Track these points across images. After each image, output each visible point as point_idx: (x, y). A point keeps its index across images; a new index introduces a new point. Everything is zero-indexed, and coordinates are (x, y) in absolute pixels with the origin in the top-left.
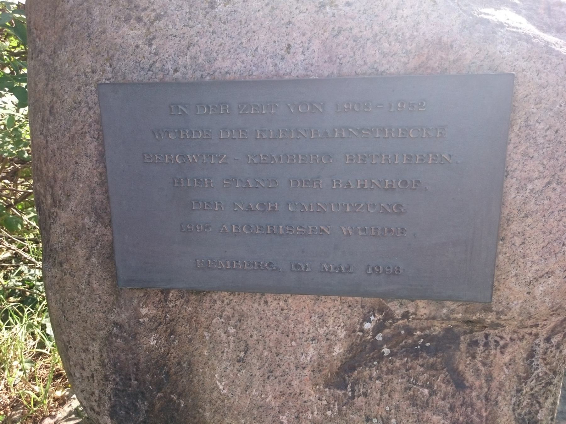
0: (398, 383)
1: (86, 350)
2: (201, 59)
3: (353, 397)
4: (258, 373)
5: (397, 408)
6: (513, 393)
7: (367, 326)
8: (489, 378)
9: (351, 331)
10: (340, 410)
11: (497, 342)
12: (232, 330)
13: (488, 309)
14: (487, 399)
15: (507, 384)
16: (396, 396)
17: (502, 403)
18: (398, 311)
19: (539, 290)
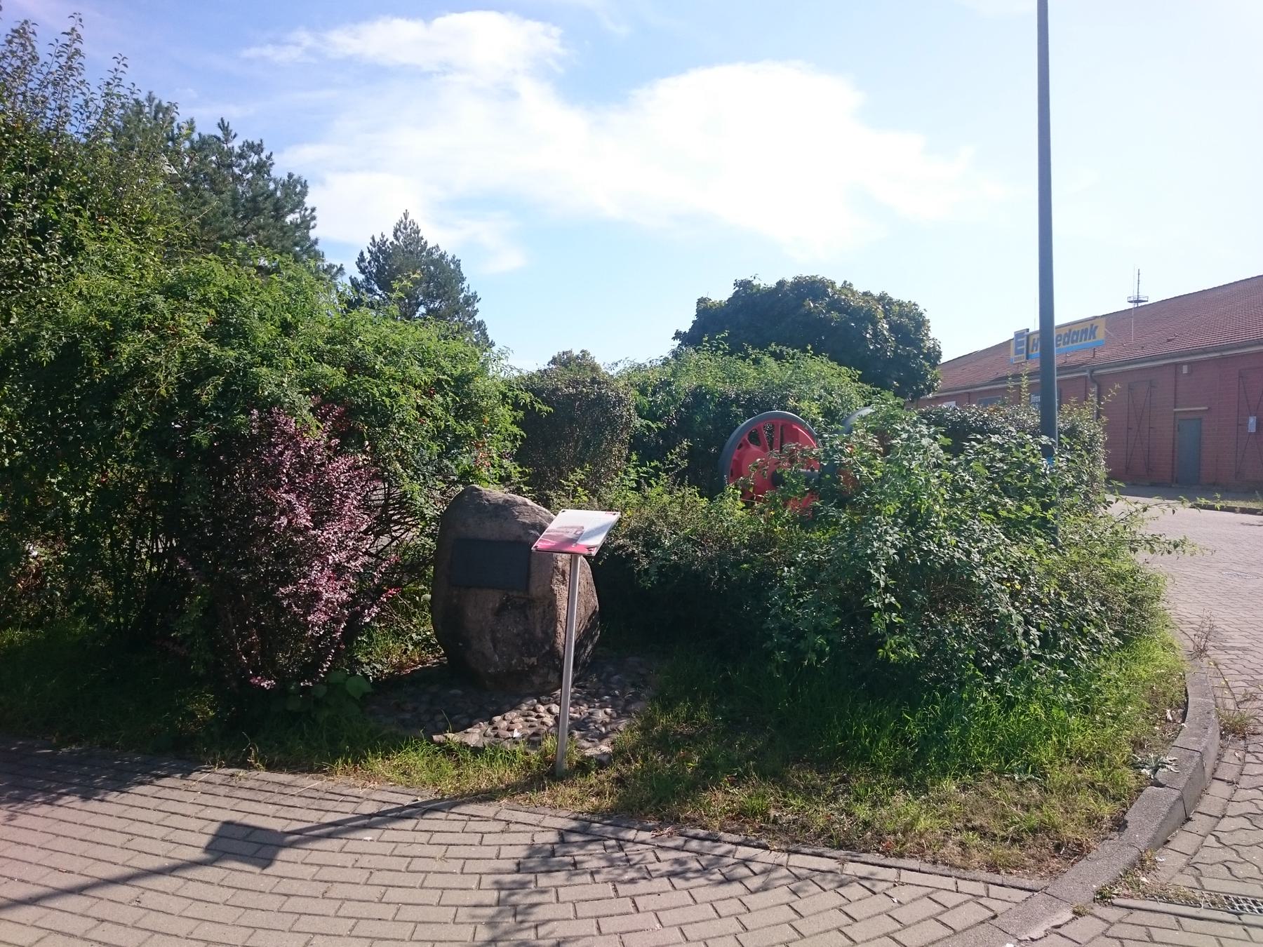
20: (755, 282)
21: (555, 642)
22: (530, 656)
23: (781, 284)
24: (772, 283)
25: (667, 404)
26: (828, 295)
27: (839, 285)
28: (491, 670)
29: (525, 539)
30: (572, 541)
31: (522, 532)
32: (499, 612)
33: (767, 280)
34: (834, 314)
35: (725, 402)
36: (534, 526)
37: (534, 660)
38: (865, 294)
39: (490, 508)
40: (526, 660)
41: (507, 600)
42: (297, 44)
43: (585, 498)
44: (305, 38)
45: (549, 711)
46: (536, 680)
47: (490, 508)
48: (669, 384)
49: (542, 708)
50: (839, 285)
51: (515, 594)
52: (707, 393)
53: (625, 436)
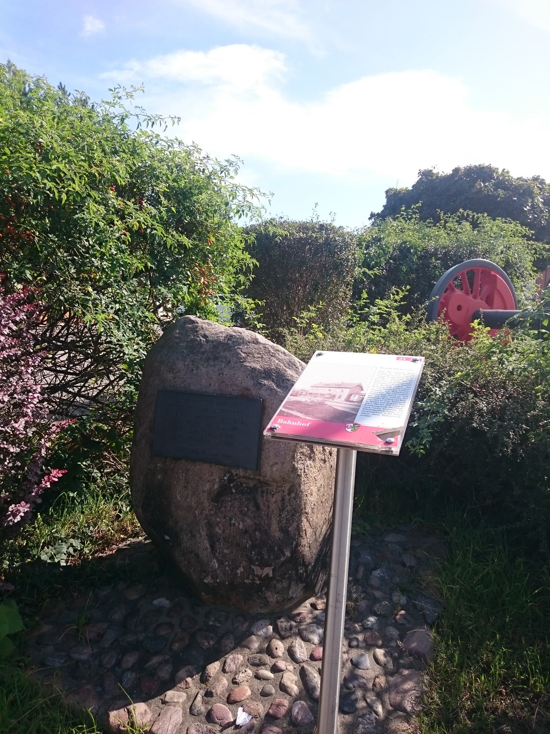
0: (237, 504)
1: (139, 479)
2: (187, 385)
3: (220, 507)
4: (190, 493)
5: (235, 514)
6: (278, 515)
7: (226, 478)
8: (268, 507)
9: (220, 480)
10: (216, 511)
11: (271, 493)
12: (184, 475)
13: (260, 475)
14: (268, 516)
15: (275, 511)
16: (236, 509)
17: (273, 519)
18: (234, 473)
19: (274, 469)
20: (435, 171)
21: (298, 545)
22: (263, 565)
23: (456, 170)
24: (449, 171)
25: (379, 256)
26: (493, 178)
27: (500, 171)
28: (208, 580)
29: (254, 392)
30: (345, 418)
31: (250, 383)
32: (218, 497)
33: (444, 169)
34: (501, 192)
35: (426, 256)
36: (267, 374)
37: (268, 571)
38: (518, 178)
39: (207, 347)
40: (257, 570)
41: (230, 480)
42: (131, 69)
43: (320, 335)
44: (136, 65)
45: (291, 653)
46: (272, 598)
47: (207, 347)
48: (380, 240)
49: (280, 647)
50: (500, 171)
51: (241, 472)
52: (411, 247)
53: (349, 279)
